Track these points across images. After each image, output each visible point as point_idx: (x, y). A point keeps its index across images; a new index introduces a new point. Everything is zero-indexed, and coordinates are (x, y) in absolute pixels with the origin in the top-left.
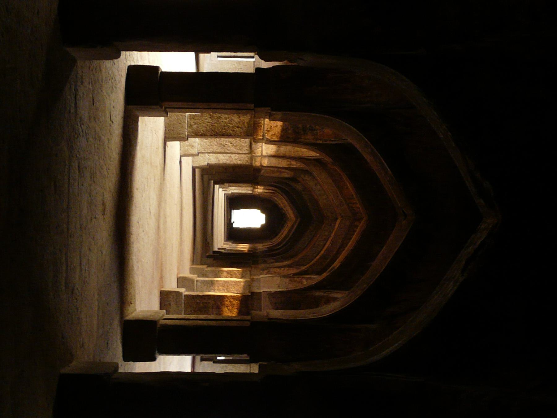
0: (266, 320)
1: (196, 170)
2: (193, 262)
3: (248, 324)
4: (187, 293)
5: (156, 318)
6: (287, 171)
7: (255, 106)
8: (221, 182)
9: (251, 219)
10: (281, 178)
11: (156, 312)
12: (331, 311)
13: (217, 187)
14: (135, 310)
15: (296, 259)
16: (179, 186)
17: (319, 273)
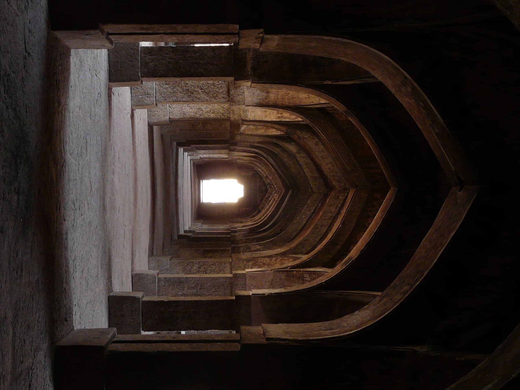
0: (264, 341)
1: (155, 128)
2: (151, 253)
3: (237, 347)
4: (145, 299)
5: (103, 341)
6: (277, 126)
7: (241, 28)
8: (189, 143)
9: (224, 191)
10: (268, 136)
11: (103, 332)
12: (357, 327)
13: (181, 150)
14: (73, 329)
15: (293, 245)
16: (131, 136)
17: (331, 265)
